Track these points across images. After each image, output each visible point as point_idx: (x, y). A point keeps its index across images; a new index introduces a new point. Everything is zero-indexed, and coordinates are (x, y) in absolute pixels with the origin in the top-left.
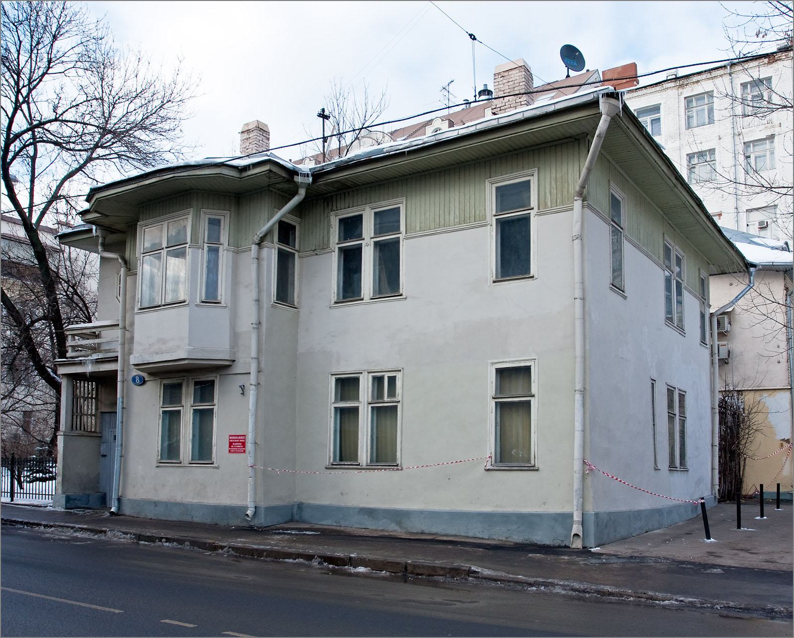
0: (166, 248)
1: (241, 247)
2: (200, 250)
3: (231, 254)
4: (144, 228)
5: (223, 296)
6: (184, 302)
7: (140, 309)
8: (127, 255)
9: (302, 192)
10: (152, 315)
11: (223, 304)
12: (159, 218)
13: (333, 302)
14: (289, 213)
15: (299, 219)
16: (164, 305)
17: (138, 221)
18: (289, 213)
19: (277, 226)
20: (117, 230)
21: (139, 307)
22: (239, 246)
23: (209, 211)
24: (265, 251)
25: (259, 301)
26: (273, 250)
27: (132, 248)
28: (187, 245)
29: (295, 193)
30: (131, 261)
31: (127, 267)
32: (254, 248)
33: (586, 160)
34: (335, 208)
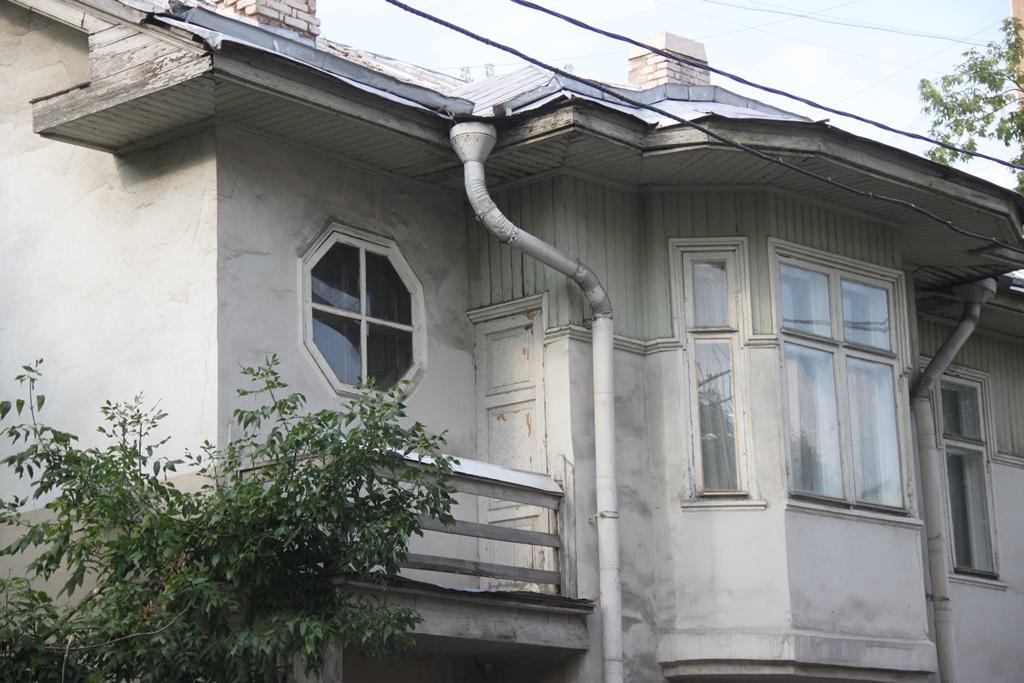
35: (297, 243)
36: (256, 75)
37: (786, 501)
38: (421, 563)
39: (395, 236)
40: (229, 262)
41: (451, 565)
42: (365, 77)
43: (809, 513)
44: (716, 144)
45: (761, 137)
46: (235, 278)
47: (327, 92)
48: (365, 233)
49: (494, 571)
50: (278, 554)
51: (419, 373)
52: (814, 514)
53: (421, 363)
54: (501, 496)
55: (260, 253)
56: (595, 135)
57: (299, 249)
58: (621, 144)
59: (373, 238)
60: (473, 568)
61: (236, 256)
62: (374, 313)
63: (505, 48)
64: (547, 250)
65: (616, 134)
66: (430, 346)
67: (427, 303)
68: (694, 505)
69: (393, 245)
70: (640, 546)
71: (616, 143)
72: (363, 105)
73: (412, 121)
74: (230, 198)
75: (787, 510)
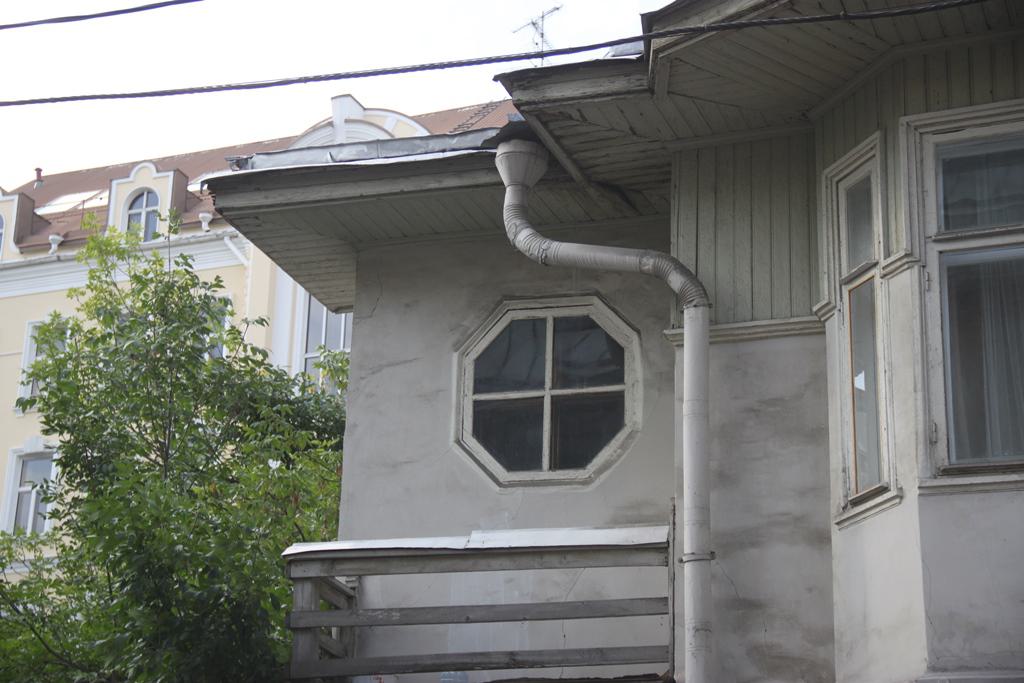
35: (454, 338)
36: (266, 198)
37: (918, 492)
38: (416, 665)
39: (600, 290)
40: (363, 382)
41: (468, 660)
42: (420, 147)
43: (987, 491)
44: (675, 44)
45: (713, 12)
46: (371, 395)
47: (355, 182)
48: (553, 300)
49: (546, 658)
50: (105, 674)
51: (631, 436)
52: (995, 491)
53: (635, 423)
54: (536, 565)
55: (406, 362)
56: (558, 104)
57: (454, 345)
58: (609, 98)
59: (565, 301)
60: (506, 660)
61: (373, 373)
62: (541, 385)
63: (423, 68)
64: (592, 254)
65: (589, 91)
66: (646, 400)
67: (644, 353)
68: (843, 518)
69: (596, 300)
70: (810, 590)
71: (596, 100)
72: (407, 177)
73: (479, 170)
74: (371, 316)
75: (920, 495)
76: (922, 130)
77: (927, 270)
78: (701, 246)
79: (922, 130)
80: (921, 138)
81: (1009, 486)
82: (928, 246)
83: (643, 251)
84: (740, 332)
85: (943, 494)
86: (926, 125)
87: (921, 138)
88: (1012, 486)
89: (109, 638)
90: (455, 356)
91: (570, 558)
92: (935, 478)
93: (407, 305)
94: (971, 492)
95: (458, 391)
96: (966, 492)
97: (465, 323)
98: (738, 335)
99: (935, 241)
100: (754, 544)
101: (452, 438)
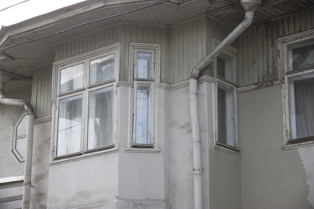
0: (88, 88)
1: (174, 83)
2: (130, 88)
3: (163, 91)
4: (60, 68)
5: (156, 139)
6: (112, 147)
7: (56, 159)
8: (33, 101)
9: (249, 15)
10: (72, 167)
11: (156, 149)
12: (77, 57)
13: (285, 142)
14: (230, 45)
15: (236, 50)
16: (86, 153)
17: (53, 61)
18: (230, 45)
19: (216, 60)
20: (20, 75)
21: (55, 157)
22: (172, 82)
23: (139, 44)
24: (205, 86)
25: (200, 142)
26: (213, 84)
27: (39, 93)
28: (115, 84)
29: (242, 18)
30: (38, 108)
31: (34, 114)
32: (193, 82)
33: (222, 40)
34: (281, 32)
35: (12, 122)
76: (58, 66)
77: (56, 105)
78: (38, 96)
79: (58, 66)
80: (58, 68)
81: (65, 162)
82: (57, 98)
83: (20, 100)
84: (43, 120)
85: (54, 165)
86: (59, 65)
87: (58, 68)
88: (66, 162)
89: (171, 192)
90: (12, 126)
91: (9, 185)
92: (53, 161)
93: (3, 113)
94: (59, 164)
95: (13, 136)
96: (58, 164)
97: (15, 117)
98: (43, 121)
99: (59, 96)
100: (43, 178)
101: (11, 150)
